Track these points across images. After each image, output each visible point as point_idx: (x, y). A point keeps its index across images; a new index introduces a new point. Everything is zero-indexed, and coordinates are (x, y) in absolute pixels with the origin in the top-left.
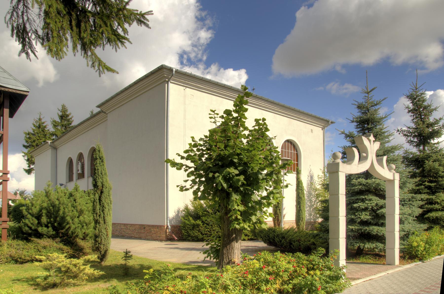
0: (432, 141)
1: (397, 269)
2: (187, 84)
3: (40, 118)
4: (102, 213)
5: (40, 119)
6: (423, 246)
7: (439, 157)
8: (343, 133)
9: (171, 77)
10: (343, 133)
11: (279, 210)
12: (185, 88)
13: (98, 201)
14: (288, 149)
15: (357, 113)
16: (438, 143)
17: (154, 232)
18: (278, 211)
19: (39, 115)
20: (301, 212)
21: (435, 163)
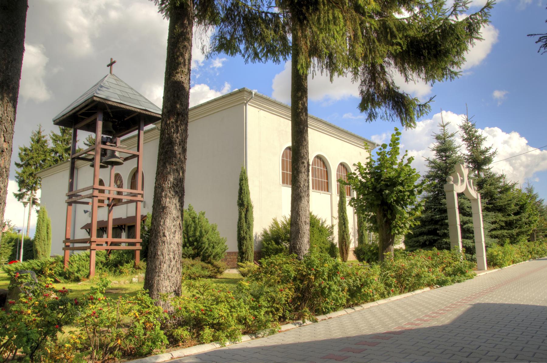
0: (485, 167)
1: (486, 273)
2: (262, 106)
3: (39, 131)
4: (248, 230)
5: (39, 133)
6: (501, 254)
7: (493, 181)
8: (428, 160)
9: (250, 99)
10: (428, 160)
11: (347, 234)
12: (259, 110)
13: (244, 219)
14: (342, 173)
15: (436, 144)
16: (489, 169)
17: (230, 260)
18: (345, 236)
19: (39, 128)
20: (363, 237)
21: (491, 186)
